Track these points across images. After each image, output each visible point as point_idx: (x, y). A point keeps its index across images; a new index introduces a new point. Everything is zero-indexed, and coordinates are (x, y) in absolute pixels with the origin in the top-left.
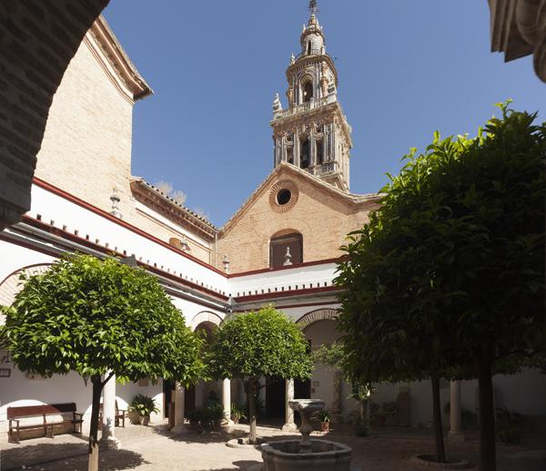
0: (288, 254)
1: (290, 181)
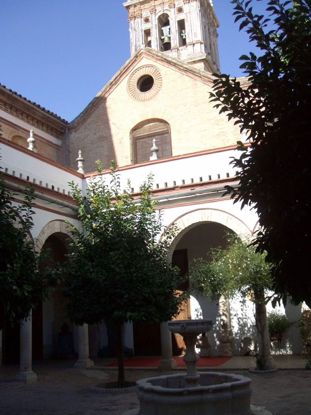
0: (154, 147)
1: (152, 66)
